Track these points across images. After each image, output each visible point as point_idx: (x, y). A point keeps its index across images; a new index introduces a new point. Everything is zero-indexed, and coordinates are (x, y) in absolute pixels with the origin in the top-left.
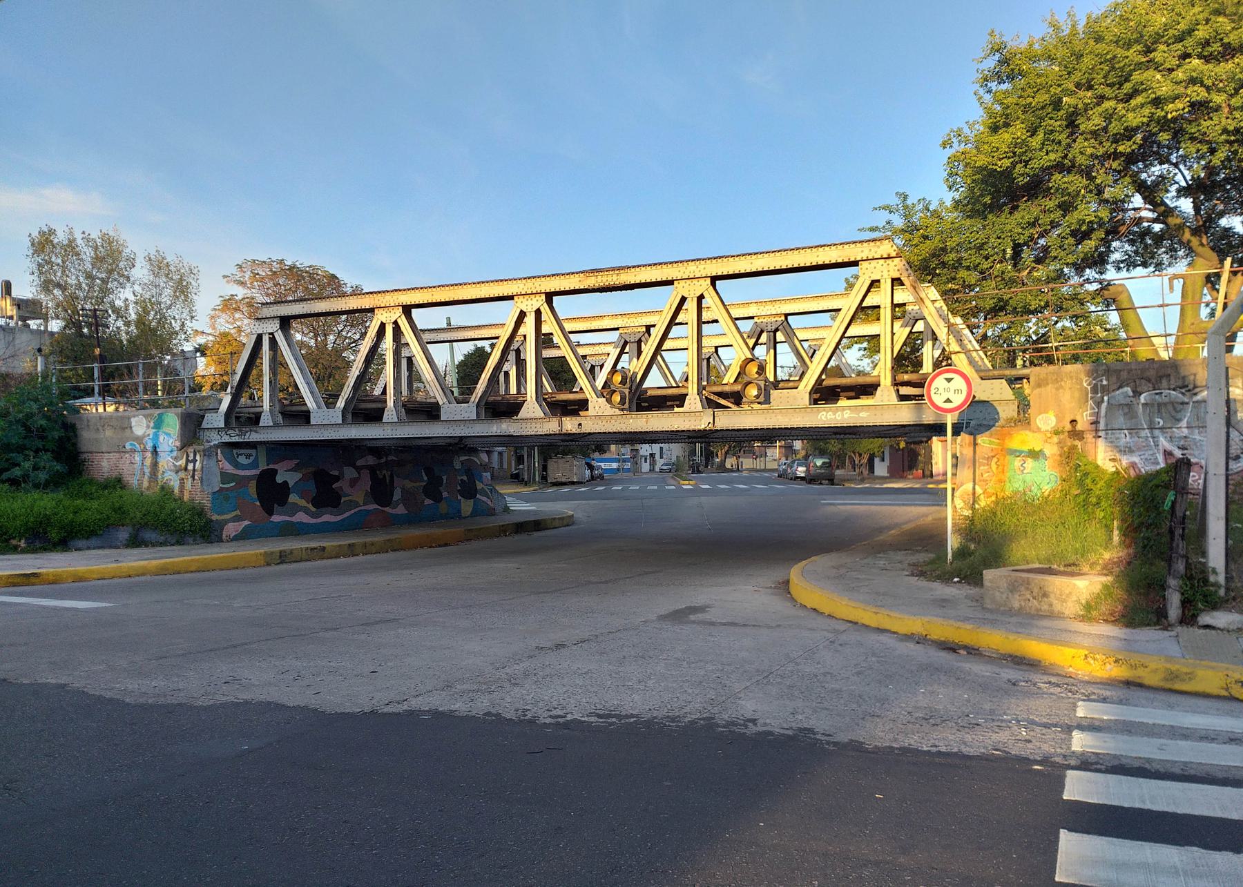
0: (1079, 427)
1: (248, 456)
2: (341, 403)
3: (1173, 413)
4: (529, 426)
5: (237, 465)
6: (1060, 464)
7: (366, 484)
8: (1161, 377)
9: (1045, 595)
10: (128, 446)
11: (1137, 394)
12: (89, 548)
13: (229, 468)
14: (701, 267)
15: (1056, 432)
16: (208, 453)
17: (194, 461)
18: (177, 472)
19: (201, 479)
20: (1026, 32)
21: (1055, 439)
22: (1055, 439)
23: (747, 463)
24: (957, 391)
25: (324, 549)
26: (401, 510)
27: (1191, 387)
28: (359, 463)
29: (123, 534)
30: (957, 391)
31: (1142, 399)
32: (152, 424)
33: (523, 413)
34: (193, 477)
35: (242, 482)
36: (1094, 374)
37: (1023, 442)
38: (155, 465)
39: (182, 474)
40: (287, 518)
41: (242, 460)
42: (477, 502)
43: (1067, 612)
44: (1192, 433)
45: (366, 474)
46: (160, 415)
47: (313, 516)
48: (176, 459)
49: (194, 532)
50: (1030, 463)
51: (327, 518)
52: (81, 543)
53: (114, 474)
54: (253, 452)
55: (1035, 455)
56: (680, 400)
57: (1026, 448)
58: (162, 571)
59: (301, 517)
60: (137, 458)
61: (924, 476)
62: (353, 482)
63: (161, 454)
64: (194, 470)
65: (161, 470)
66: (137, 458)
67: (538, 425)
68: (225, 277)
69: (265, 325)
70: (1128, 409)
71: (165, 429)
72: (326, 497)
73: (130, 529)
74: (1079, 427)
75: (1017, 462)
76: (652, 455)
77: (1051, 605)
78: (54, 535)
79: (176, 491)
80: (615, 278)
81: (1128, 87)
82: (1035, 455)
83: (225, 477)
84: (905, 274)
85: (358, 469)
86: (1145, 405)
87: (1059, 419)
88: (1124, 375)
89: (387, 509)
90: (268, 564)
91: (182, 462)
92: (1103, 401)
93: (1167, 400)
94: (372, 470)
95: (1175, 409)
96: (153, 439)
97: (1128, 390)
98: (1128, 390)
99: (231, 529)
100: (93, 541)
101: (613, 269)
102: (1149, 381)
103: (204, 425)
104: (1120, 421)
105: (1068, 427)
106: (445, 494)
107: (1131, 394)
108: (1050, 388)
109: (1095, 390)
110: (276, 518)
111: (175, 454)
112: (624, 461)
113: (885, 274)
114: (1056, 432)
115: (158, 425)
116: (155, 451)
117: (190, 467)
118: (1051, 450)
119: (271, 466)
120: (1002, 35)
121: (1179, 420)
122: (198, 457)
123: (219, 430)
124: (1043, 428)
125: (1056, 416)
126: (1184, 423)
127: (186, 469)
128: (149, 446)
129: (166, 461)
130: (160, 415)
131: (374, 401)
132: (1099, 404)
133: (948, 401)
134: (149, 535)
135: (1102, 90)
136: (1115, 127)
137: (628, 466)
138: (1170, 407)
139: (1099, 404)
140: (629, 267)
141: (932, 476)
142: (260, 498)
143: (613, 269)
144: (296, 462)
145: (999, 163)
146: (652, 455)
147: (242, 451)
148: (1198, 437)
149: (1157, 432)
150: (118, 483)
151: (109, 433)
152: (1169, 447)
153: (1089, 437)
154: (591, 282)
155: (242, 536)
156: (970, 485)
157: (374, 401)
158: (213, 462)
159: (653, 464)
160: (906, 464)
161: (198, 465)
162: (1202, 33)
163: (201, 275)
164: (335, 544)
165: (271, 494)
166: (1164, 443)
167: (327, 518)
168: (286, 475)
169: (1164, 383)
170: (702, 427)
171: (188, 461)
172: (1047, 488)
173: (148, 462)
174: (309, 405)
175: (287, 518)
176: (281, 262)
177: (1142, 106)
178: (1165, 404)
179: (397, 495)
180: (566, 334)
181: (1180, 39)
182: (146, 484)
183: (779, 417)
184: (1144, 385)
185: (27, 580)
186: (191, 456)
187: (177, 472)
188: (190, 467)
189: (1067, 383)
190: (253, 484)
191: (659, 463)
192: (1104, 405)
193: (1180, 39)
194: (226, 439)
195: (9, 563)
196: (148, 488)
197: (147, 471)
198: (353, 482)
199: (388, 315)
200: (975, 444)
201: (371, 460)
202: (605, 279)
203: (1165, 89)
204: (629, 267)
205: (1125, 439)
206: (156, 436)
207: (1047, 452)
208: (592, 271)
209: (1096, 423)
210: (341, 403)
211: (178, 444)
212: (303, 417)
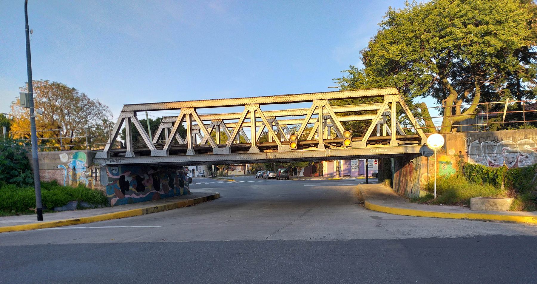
0: (462, 154)
1: (116, 170)
2: (166, 147)
4: (255, 156)
5: (113, 174)
6: (456, 166)
7: (151, 182)
9: (496, 204)
10: (59, 167)
11: (480, 142)
12: (62, 211)
13: (111, 176)
14: (324, 95)
15: (455, 156)
16: (102, 169)
17: (96, 173)
18: (87, 177)
19: (100, 180)
20: (399, 8)
21: (454, 158)
22: (454, 158)
23: (230, 173)
25: (157, 207)
26: (162, 192)
28: (149, 173)
29: (75, 205)
32: (72, 157)
33: (250, 151)
34: (96, 179)
35: (115, 181)
36: (468, 136)
37: (444, 159)
38: (74, 175)
39: (90, 178)
40: (129, 196)
41: (114, 172)
42: (185, 188)
43: (503, 209)
45: (151, 177)
46: (76, 153)
47: (138, 195)
48: (86, 172)
49: (102, 203)
50: (446, 166)
51: (141, 196)
52: (59, 209)
53: (53, 179)
54: (117, 168)
55: (448, 163)
56: (316, 145)
57: (445, 161)
58: (116, 217)
59: (134, 196)
60: (65, 172)
61: (319, 176)
62: (148, 181)
63: (77, 170)
64: (96, 176)
65: (78, 177)
66: (65, 172)
67: (257, 156)
68: (20, 88)
69: (126, 114)
70: (478, 147)
71: (79, 159)
72: (140, 188)
73: (77, 202)
74: (462, 154)
75: (442, 166)
76: (193, 170)
77: (497, 208)
78: (50, 205)
79: (87, 186)
80: (289, 98)
81: (443, 33)
82: (448, 163)
83: (110, 179)
84: (401, 100)
85: (149, 175)
86: (483, 146)
87: (456, 151)
88: (476, 136)
89: (159, 192)
90: (143, 214)
91: (90, 173)
94: (153, 175)
96: (73, 163)
97: (477, 141)
98: (477, 141)
99: (114, 201)
100: (64, 208)
101: (288, 95)
103: (96, 157)
104: (475, 151)
105: (459, 154)
106: (175, 186)
108: (453, 141)
109: (467, 141)
110: (127, 196)
111: (85, 170)
113: (394, 100)
114: (455, 156)
115: (75, 157)
116: (74, 169)
117: (94, 175)
118: (453, 161)
119: (123, 174)
120: (395, 9)
121: (493, 151)
122: (98, 171)
123: (104, 159)
124: (451, 154)
126: (495, 152)
127: (92, 176)
128: (71, 166)
129: (80, 173)
130: (76, 153)
131: (180, 147)
132: (468, 146)
134: (85, 205)
135: (434, 33)
136: (439, 47)
139: (468, 146)
140: (295, 95)
141: (323, 175)
142: (121, 187)
143: (288, 95)
144: (130, 172)
145: (397, 57)
146: (193, 170)
147: (114, 168)
148: (499, 156)
149: (487, 155)
150: (55, 183)
151: (47, 161)
152: (490, 160)
153: (465, 157)
154: (279, 100)
155: (117, 204)
156: (426, 174)
157: (180, 147)
158: (105, 173)
159: (194, 173)
160: (311, 171)
161: (98, 174)
162: (470, 15)
163: (115, 93)
164: (160, 205)
165: (124, 186)
166: (489, 158)
167: (141, 196)
168: (128, 179)
169: (489, 139)
170: (325, 155)
171: (92, 173)
172: (452, 174)
173: (71, 173)
174: (150, 148)
175: (129, 196)
176: (46, 81)
177: (449, 40)
179: (161, 187)
181: (462, 16)
182: (70, 183)
184: (482, 139)
185: (76, 222)
186: (94, 171)
187: (87, 177)
188: (94, 175)
189: (458, 139)
190: (118, 182)
191: (197, 174)
192: (470, 147)
193: (462, 16)
194: (108, 163)
195: (52, 216)
196: (72, 184)
197: (71, 178)
198: (148, 181)
199: (187, 111)
200: (428, 160)
201: (151, 172)
202: (284, 99)
203: (460, 35)
204: (295, 95)
205: (477, 157)
206: (74, 162)
207: (452, 162)
208: (280, 96)
209: (468, 152)
210: (166, 147)
211: (87, 165)
212: (148, 153)
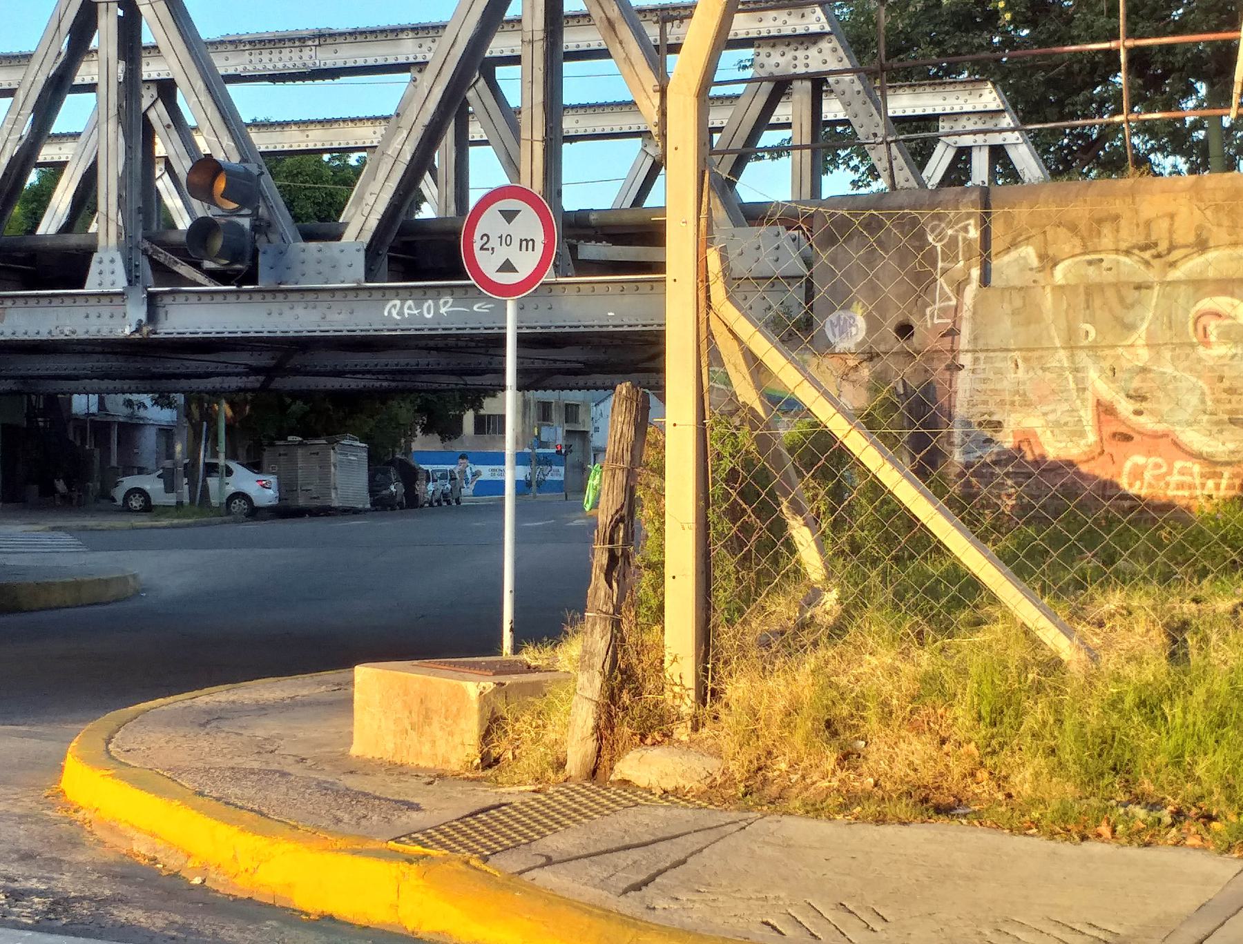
3: (1119, 310)
8: (1100, 221)
11: (1048, 261)
24: (527, 243)
27: (1163, 246)
30: (527, 243)
31: (1060, 274)
44: (1157, 357)
92: (967, 280)
93: (1109, 277)
95: (1122, 300)
102: (1073, 228)
107: (1035, 262)
112: (546, 461)
121: (1130, 328)
125: (869, 318)
133: (507, 267)
137: (557, 473)
138: (1111, 294)
148: (1169, 369)
149: (1083, 358)
169: (1107, 241)
178: (1101, 287)
180: (216, 85)
183: (300, 311)
